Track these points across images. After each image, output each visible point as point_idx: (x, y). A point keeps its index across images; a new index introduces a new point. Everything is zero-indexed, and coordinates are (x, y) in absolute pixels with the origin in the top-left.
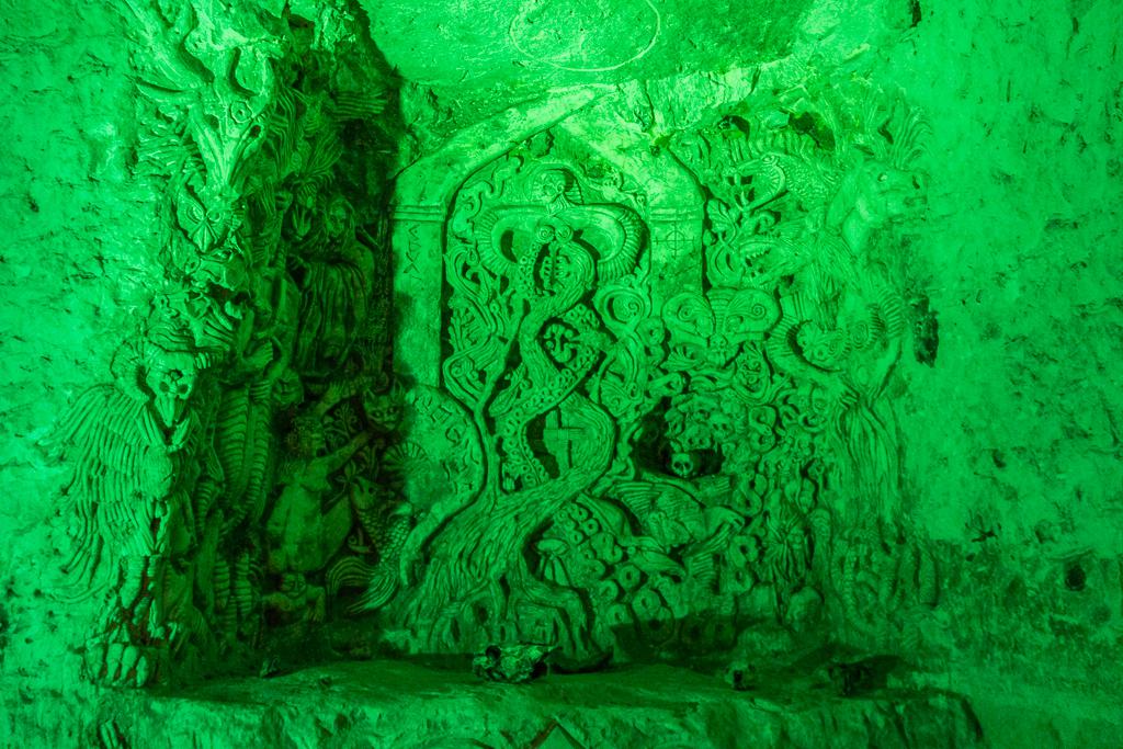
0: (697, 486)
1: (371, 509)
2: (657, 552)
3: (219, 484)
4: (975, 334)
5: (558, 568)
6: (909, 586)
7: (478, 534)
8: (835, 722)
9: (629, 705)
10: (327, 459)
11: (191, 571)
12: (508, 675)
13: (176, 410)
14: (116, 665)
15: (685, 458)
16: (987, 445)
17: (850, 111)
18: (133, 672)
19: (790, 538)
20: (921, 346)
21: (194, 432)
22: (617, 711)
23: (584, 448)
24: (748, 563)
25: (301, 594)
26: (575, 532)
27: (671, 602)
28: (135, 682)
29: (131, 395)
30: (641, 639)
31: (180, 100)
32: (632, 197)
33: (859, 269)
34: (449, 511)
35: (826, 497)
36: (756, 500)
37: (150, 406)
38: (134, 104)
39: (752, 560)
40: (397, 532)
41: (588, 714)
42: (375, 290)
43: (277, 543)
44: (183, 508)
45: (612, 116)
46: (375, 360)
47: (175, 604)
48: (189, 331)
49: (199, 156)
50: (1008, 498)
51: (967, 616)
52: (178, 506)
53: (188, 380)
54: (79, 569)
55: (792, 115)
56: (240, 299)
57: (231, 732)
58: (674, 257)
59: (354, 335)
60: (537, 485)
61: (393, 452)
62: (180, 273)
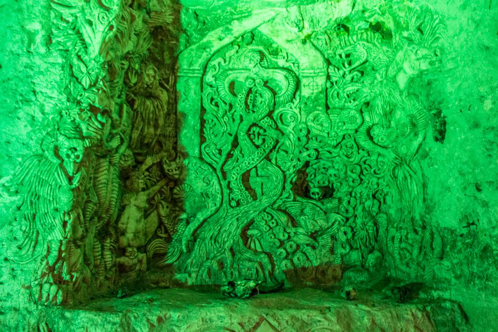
0: (323, 203)
1: (168, 216)
2: (304, 234)
3: (95, 204)
4: (466, 126)
7: (219, 227)
10: (147, 192)
11: (83, 246)
12: (239, 295)
13: (74, 167)
14: (47, 294)
15: (317, 190)
16: (472, 181)
17: (402, 20)
18: (55, 297)
19: (367, 227)
20: (437, 134)
21: (83, 179)
22: (293, 312)
23: (268, 185)
24: (347, 239)
26: (265, 226)
27: (311, 258)
28: (56, 303)
29: (52, 160)
30: (297, 275)
31: (73, 11)
32: (292, 65)
33: (404, 98)
34: (205, 216)
35: (385, 208)
36: (351, 210)
37: (61, 166)
38: (49, 13)
39: (349, 238)
40: (181, 227)
41: (279, 313)
42: (168, 110)
43: (123, 233)
44: (79, 215)
45: (283, 24)
46: (169, 145)
47: (75, 263)
48: (80, 128)
49: (83, 40)
50: (483, 206)
51: (460, 264)
53: (80, 153)
54: (27, 247)
55: (371, 23)
56: (106, 113)
57: (105, 326)
58: (312, 94)
59: (158, 132)
60: (247, 204)
61: (178, 189)
62: (75, 99)
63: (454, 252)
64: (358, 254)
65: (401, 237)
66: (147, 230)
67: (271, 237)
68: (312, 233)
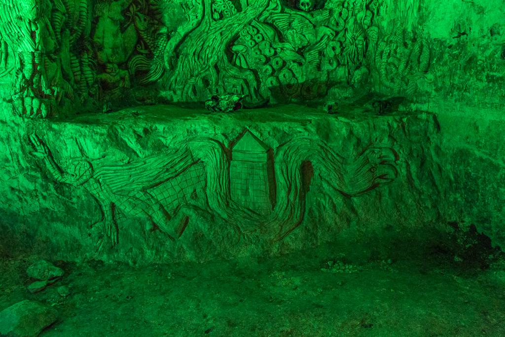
0: (312, 15)
3: (64, 14)
5: (242, 59)
6: (415, 64)
7: (202, 43)
8: (374, 126)
9: (280, 121)
11: (58, 61)
12: (223, 109)
18: (39, 111)
24: (335, 55)
25: (117, 74)
26: (250, 41)
27: (297, 75)
34: (186, 30)
35: (378, 20)
36: (342, 22)
40: (161, 42)
41: (262, 125)
43: (101, 48)
47: (54, 77)
50: (479, 13)
52: (43, 25)
57: (94, 137)
60: (231, 16)
63: (440, 65)
64: (345, 69)
65: (390, 52)
66: (126, 45)
67: (257, 53)
68: (299, 49)
